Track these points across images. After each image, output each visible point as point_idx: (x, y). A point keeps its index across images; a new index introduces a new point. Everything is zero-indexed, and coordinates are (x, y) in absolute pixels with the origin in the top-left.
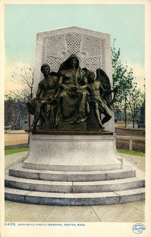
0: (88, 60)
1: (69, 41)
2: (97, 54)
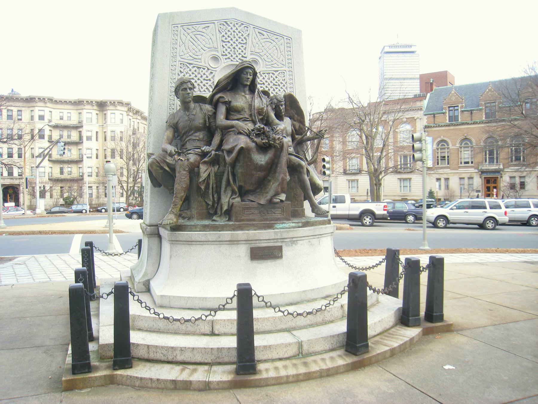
2: (279, 64)
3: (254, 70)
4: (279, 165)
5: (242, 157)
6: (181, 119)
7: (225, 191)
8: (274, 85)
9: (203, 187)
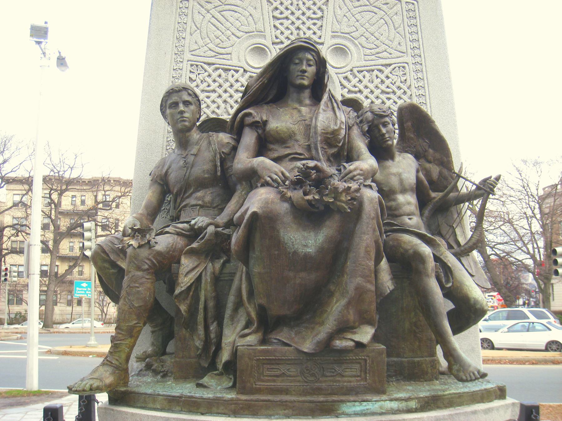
0: (357, 74)
1: (279, 6)
2: (392, 51)
3: (318, 53)
4: (351, 255)
5: (258, 236)
6: (173, 166)
7: (232, 318)
8: (383, 92)
9: (183, 308)
